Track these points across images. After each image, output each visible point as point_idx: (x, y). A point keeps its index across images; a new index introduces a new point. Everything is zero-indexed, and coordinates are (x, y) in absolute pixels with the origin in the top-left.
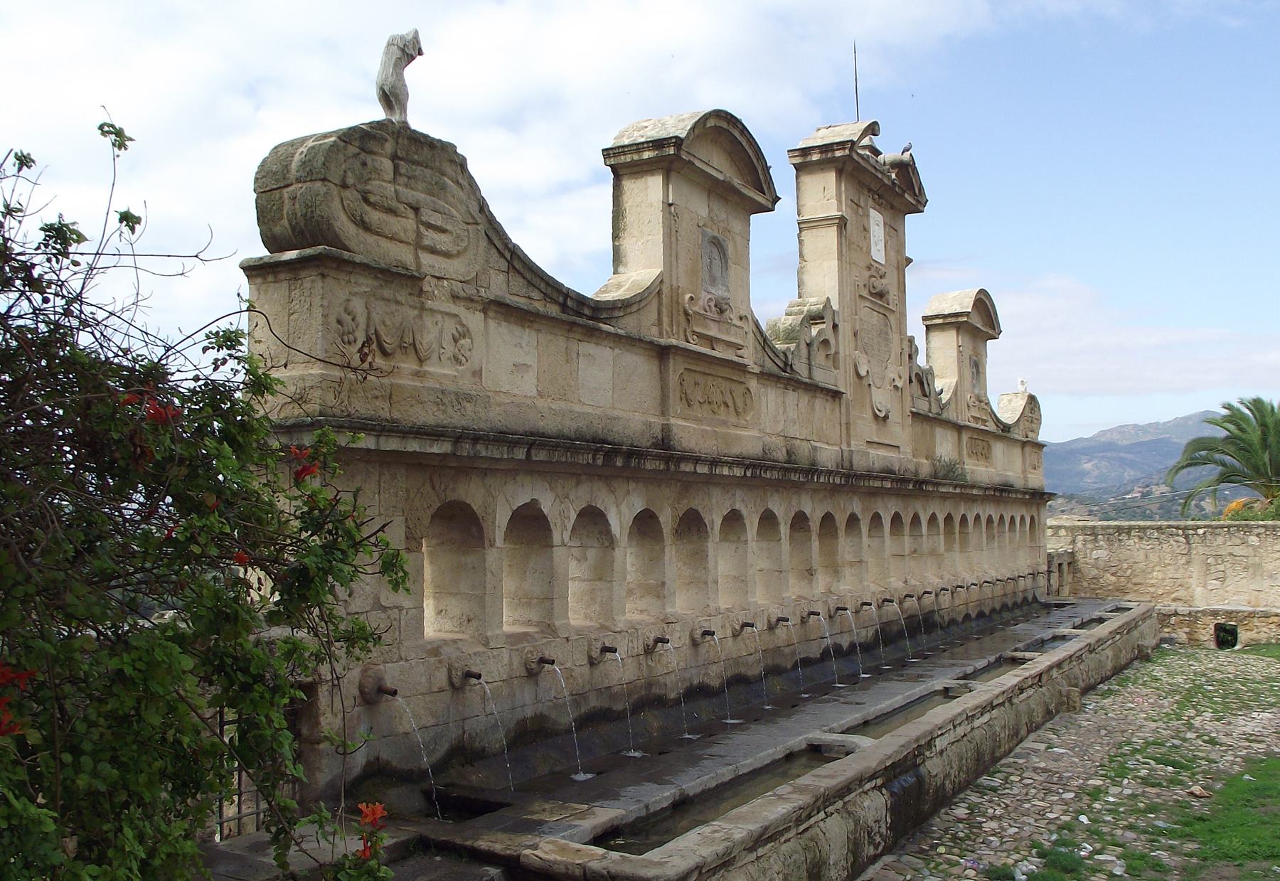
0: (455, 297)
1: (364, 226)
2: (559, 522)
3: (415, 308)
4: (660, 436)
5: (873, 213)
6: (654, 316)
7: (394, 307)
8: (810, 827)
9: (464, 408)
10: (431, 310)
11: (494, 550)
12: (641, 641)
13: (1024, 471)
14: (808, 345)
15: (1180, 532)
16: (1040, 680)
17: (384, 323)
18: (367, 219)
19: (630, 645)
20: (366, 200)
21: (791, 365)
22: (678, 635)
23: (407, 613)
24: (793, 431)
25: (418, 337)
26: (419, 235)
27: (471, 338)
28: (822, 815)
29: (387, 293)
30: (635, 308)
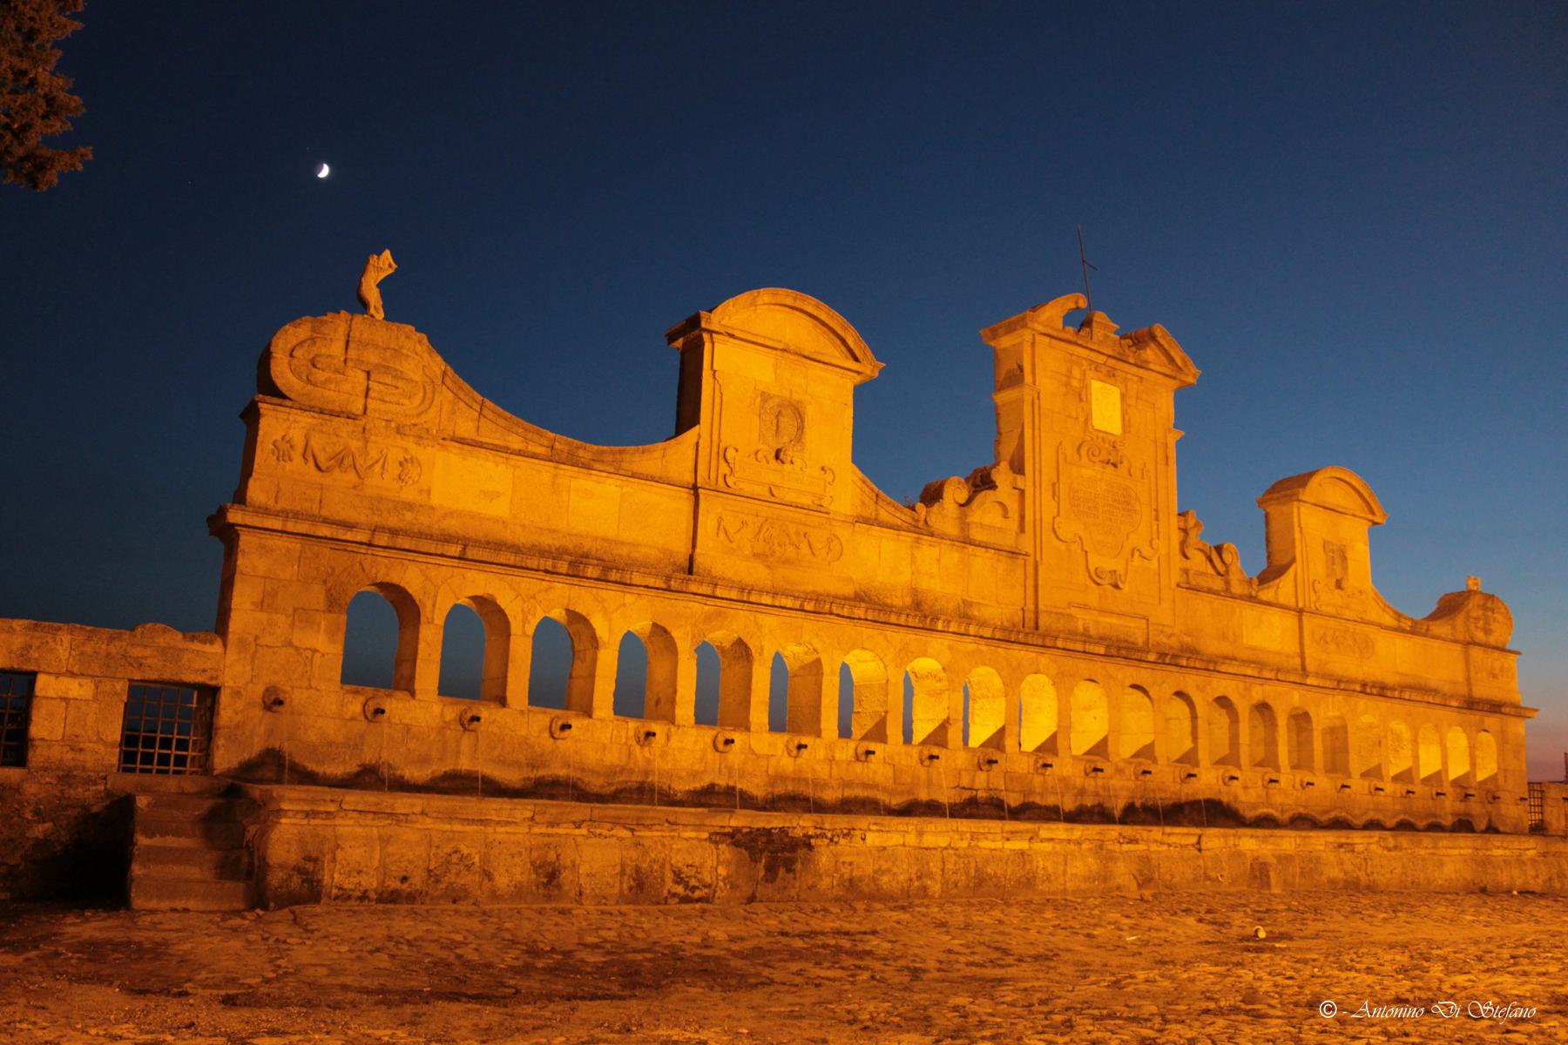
2: (520, 617)
3: (358, 440)
5: (1096, 386)
6: (691, 464)
7: (335, 439)
9: (404, 515)
10: (376, 442)
11: (432, 626)
13: (1468, 679)
16: (1199, 843)
17: (324, 449)
18: (312, 378)
19: (615, 733)
21: (926, 521)
22: (693, 739)
23: (323, 655)
24: (925, 584)
25: (359, 461)
27: (420, 465)
28: (584, 831)
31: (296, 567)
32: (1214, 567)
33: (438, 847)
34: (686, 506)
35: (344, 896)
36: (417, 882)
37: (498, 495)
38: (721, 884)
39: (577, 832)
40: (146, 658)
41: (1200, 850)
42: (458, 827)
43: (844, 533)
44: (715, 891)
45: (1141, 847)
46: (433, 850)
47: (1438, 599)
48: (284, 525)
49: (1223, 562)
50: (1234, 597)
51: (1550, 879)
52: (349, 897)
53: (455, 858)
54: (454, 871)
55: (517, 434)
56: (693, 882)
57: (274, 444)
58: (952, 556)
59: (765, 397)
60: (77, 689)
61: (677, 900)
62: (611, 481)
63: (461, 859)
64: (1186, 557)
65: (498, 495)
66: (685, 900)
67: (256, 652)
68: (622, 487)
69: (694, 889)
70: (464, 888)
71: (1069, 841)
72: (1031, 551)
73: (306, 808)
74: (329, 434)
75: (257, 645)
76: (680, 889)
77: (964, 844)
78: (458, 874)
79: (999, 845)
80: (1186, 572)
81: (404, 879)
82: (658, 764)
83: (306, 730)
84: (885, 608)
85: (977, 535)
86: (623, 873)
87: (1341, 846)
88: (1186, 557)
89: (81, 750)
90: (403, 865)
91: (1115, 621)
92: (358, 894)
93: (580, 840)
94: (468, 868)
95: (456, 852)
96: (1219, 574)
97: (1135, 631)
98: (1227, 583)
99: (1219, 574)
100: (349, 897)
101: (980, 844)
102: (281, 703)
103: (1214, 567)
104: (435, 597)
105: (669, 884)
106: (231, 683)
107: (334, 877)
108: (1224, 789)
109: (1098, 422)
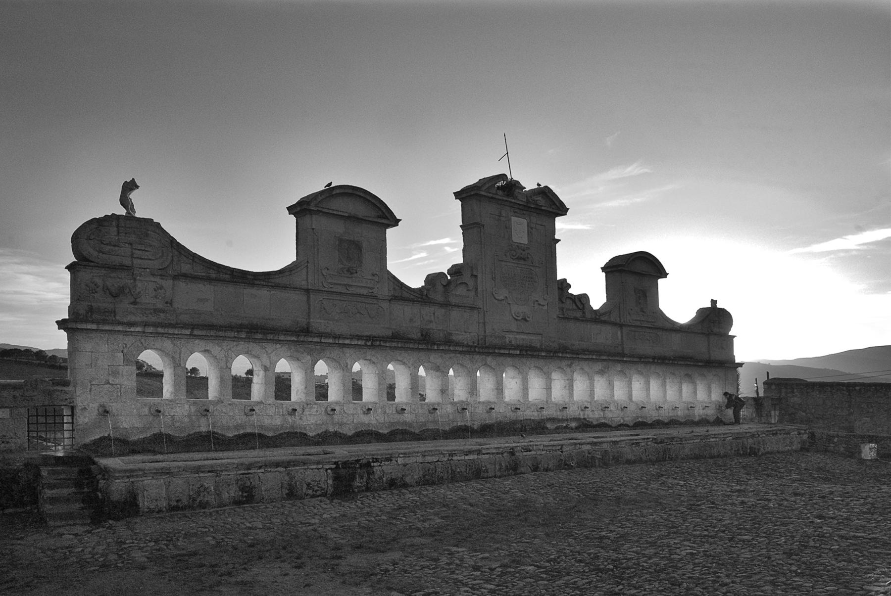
0: (153, 275)
1: (100, 252)
4: (305, 327)
5: (514, 219)
8: (249, 473)
12: (285, 409)
14: (444, 286)
15: (844, 388)
20: (102, 243)
26: (133, 254)
29: (112, 275)
30: (287, 274)
31: (106, 345)
32: (577, 305)
33: (193, 485)
34: (305, 298)
35: (151, 511)
36: (185, 501)
37: (207, 300)
38: (330, 488)
39: (259, 471)
40: (34, 396)
41: (562, 452)
42: (201, 475)
43: (385, 305)
44: (327, 491)
45: (533, 453)
46: (191, 487)
47: (696, 311)
48: (98, 327)
49: (582, 303)
50: (587, 321)
51: (738, 450)
52: (153, 511)
53: (202, 489)
54: (202, 495)
55: (213, 269)
56: (316, 488)
57: (87, 285)
58: (440, 312)
59: (341, 241)
60: (44, 474)
61: (309, 497)
62: (264, 289)
63: (205, 490)
64: (563, 302)
65: (207, 300)
66: (313, 496)
67: (91, 389)
68: (270, 292)
69: (316, 491)
70: (207, 502)
71: (497, 453)
72: (481, 307)
73: (127, 474)
74: (115, 278)
75: (91, 385)
76: (310, 492)
77: (446, 459)
78: (204, 496)
79: (463, 458)
80: (562, 309)
81: (177, 501)
82: (298, 422)
83: (122, 422)
84: (410, 340)
85: (453, 300)
86: (282, 487)
87: (633, 444)
88: (563, 302)
89: (8, 442)
90: (177, 495)
91: (524, 337)
92: (157, 510)
93: (260, 474)
94: (208, 493)
95: (202, 486)
96: (579, 309)
97: (535, 341)
98: (584, 313)
99: (579, 309)
100: (153, 511)
101: (453, 458)
102: (107, 412)
103: (577, 305)
104: (180, 354)
105: (304, 489)
106: (81, 404)
107: (144, 503)
108: (582, 413)
109: (515, 239)
